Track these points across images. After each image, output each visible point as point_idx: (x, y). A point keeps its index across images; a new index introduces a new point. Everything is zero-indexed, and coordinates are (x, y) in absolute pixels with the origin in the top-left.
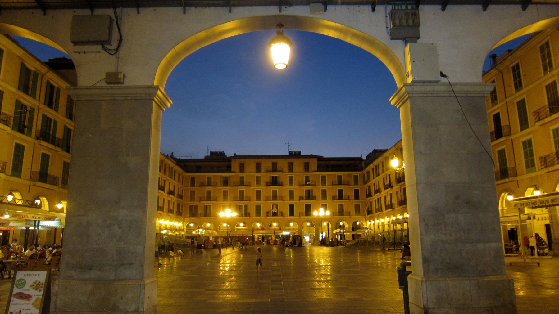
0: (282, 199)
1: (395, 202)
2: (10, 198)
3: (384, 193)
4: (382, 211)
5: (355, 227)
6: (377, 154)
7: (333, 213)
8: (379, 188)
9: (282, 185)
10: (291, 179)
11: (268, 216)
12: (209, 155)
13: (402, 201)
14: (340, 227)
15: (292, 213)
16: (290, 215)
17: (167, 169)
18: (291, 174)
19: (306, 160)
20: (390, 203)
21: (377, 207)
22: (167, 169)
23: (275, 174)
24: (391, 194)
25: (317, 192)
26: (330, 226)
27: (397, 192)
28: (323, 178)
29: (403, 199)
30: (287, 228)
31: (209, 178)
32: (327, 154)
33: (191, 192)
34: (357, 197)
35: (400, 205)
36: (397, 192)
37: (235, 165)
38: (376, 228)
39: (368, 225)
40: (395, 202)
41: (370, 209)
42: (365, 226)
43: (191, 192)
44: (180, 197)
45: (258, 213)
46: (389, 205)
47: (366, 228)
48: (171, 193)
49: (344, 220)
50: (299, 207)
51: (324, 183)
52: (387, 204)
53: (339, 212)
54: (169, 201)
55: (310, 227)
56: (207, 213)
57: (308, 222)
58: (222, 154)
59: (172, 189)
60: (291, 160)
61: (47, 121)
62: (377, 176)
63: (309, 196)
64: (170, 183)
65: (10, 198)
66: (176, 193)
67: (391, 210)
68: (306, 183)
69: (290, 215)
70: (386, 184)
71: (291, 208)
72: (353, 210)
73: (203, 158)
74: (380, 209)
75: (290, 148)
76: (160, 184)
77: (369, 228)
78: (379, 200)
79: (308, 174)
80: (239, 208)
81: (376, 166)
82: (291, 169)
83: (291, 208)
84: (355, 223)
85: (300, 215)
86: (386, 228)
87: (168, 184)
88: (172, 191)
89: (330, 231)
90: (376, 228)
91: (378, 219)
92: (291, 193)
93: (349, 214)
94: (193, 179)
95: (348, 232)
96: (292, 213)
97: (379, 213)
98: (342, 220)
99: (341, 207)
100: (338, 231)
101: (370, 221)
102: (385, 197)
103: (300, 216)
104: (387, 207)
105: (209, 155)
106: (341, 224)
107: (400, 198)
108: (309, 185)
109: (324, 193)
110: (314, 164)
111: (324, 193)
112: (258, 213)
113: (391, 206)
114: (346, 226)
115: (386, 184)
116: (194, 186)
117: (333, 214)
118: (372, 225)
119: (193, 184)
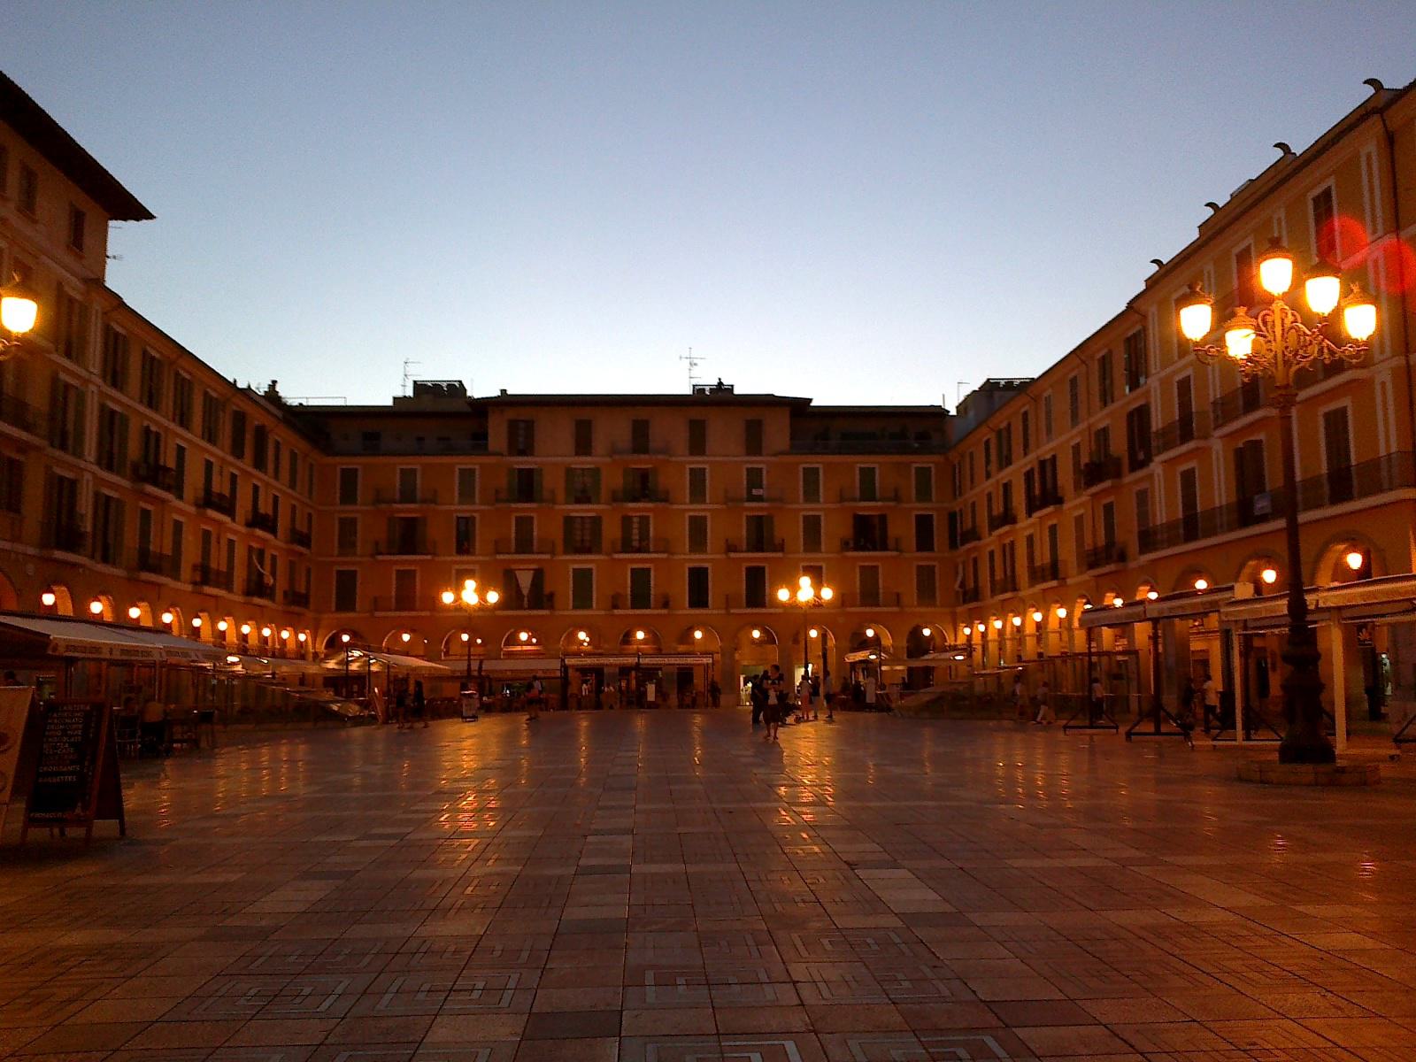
0: (666, 546)
1: (1068, 553)
2: (48, 599)
3: (1026, 525)
4: (1015, 589)
5: (918, 646)
6: (997, 394)
7: (843, 595)
8: (974, 527)
9: (666, 500)
10: (698, 477)
11: (615, 607)
12: (410, 392)
13: (1095, 552)
14: (864, 644)
15: (699, 597)
16: (693, 605)
17: (249, 438)
18: (698, 462)
19: (752, 414)
20: (1047, 559)
21: (999, 575)
22: (249, 438)
23: (643, 462)
24: (1053, 529)
25: (790, 529)
26: (832, 642)
27: (1079, 520)
28: (811, 474)
29: (1101, 541)
30: (682, 648)
31: (408, 475)
32: (831, 389)
33: (343, 522)
34: (925, 542)
35: (1091, 566)
36: (1079, 520)
37: (497, 434)
38: (993, 647)
39: (961, 641)
40: (1068, 553)
41: (971, 585)
42: (950, 641)
43: (343, 522)
44: (302, 539)
45: (583, 597)
46: (1043, 569)
47: (954, 648)
48: (260, 521)
49: (877, 622)
50: (726, 583)
51: (811, 493)
52: (1038, 563)
53: (862, 594)
54: (207, 534)
55: (759, 643)
56: (411, 600)
57: (754, 628)
58: (457, 389)
59: (265, 508)
60: (696, 413)
61: (111, 422)
62: (1001, 468)
63: (761, 536)
64: (256, 488)
65: (48, 599)
66: (283, 524)
67: (1054, 583)
68: (749, 492)
69: (693, 605)
70: (995, 513)
71: (698, 579)
72: (910, 591)
73: (390, 403)
74: (1011, 584)
75: (696, 371)
76: (216, 488)
77: (968, 648)
78: (1009, 551)
79: (757, 461)
80: (507, 581)
81: (999, 433)
82: (697, 445)
83: (698, 579)
84: (916, 632)
85: (729, 602)
86: (1030, 645)
87: (250, 491)
88: (265, 517)
89: (832, 659)
90: (993, 647)
91: (1002, 613)
92: (698, 529)
93: (898, 599)
94: (349, 478)
95: (895, 660)
96: (699, 597)
97: (1008, 595)
98: (872, 621)
99: (869, 574)
100: (860, 656)
101: (970, 625)
102: (1030, 539)
103: (727, 608)
104: (1036, 575)
105: (410, 392)
106: (870, 633)
107: (1088, 540)
108: (759, 499)
109: (812, 525)
110: (777, 432)
111: (812, 525)
112: (583, 597)
113: (1055, 570)
114: (887, 641)
115: (995, 513)
116: (354, 502)
117: (842, 600)
118: (977, 640)
119: (348, 495)
